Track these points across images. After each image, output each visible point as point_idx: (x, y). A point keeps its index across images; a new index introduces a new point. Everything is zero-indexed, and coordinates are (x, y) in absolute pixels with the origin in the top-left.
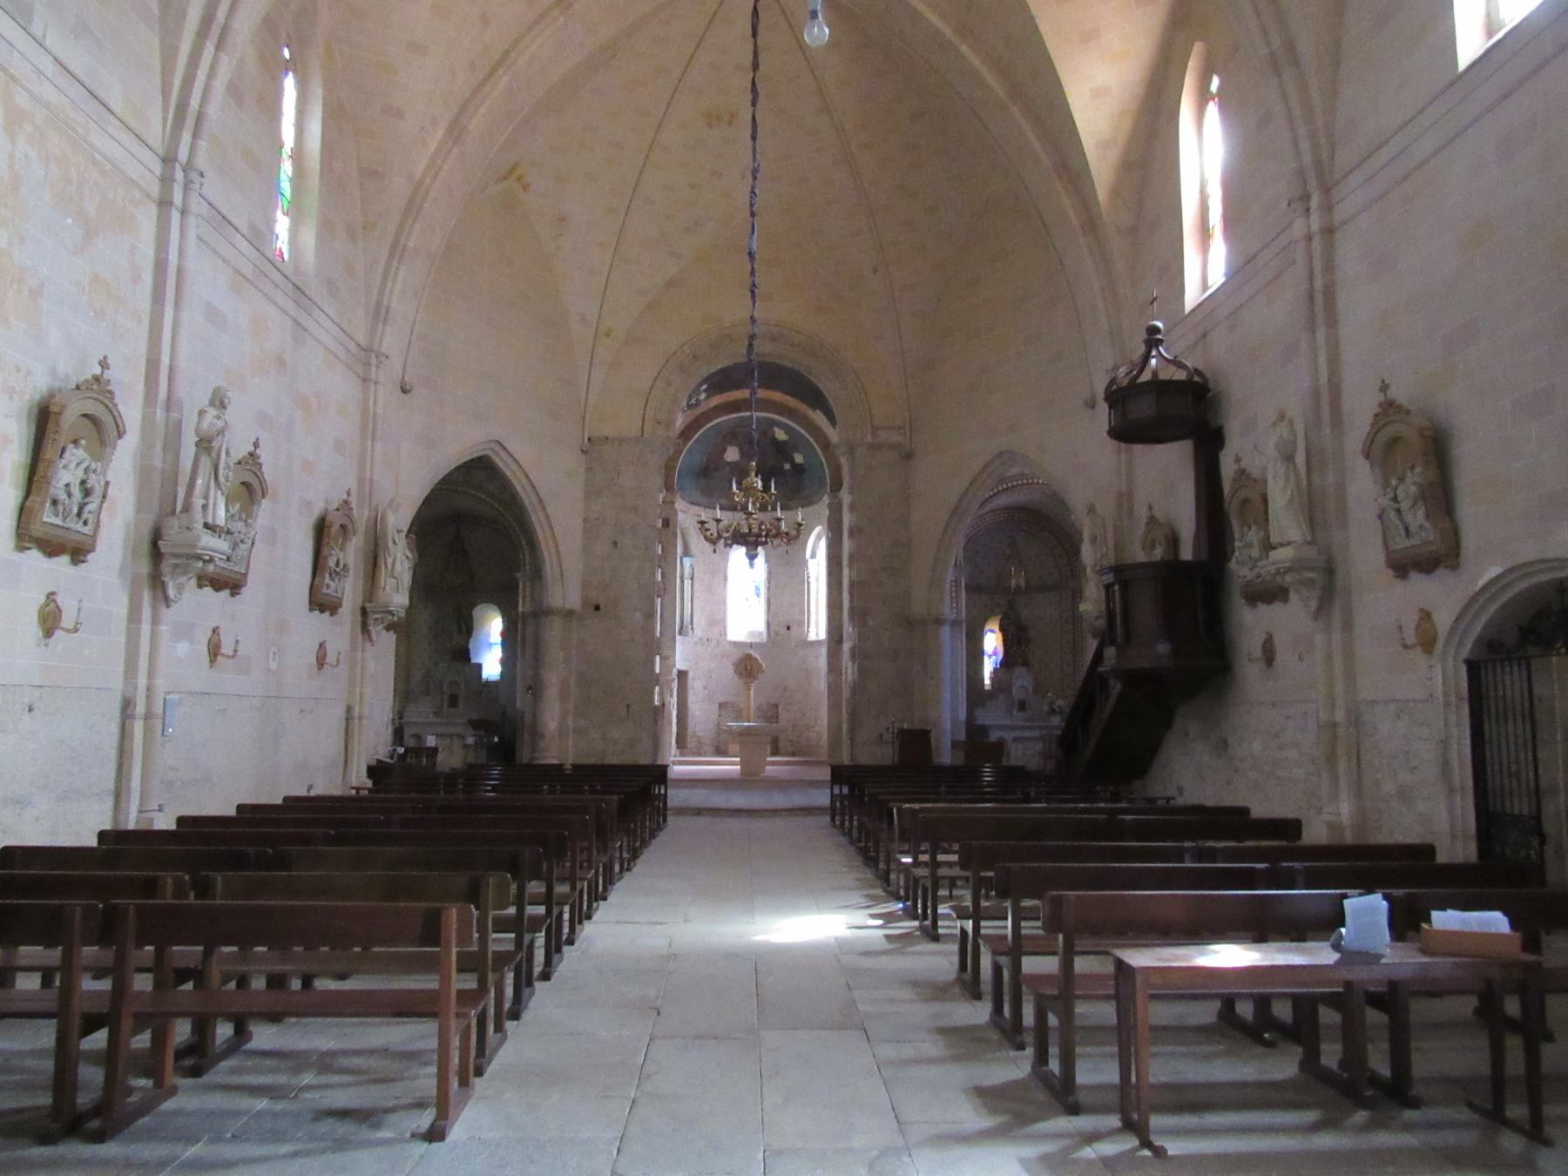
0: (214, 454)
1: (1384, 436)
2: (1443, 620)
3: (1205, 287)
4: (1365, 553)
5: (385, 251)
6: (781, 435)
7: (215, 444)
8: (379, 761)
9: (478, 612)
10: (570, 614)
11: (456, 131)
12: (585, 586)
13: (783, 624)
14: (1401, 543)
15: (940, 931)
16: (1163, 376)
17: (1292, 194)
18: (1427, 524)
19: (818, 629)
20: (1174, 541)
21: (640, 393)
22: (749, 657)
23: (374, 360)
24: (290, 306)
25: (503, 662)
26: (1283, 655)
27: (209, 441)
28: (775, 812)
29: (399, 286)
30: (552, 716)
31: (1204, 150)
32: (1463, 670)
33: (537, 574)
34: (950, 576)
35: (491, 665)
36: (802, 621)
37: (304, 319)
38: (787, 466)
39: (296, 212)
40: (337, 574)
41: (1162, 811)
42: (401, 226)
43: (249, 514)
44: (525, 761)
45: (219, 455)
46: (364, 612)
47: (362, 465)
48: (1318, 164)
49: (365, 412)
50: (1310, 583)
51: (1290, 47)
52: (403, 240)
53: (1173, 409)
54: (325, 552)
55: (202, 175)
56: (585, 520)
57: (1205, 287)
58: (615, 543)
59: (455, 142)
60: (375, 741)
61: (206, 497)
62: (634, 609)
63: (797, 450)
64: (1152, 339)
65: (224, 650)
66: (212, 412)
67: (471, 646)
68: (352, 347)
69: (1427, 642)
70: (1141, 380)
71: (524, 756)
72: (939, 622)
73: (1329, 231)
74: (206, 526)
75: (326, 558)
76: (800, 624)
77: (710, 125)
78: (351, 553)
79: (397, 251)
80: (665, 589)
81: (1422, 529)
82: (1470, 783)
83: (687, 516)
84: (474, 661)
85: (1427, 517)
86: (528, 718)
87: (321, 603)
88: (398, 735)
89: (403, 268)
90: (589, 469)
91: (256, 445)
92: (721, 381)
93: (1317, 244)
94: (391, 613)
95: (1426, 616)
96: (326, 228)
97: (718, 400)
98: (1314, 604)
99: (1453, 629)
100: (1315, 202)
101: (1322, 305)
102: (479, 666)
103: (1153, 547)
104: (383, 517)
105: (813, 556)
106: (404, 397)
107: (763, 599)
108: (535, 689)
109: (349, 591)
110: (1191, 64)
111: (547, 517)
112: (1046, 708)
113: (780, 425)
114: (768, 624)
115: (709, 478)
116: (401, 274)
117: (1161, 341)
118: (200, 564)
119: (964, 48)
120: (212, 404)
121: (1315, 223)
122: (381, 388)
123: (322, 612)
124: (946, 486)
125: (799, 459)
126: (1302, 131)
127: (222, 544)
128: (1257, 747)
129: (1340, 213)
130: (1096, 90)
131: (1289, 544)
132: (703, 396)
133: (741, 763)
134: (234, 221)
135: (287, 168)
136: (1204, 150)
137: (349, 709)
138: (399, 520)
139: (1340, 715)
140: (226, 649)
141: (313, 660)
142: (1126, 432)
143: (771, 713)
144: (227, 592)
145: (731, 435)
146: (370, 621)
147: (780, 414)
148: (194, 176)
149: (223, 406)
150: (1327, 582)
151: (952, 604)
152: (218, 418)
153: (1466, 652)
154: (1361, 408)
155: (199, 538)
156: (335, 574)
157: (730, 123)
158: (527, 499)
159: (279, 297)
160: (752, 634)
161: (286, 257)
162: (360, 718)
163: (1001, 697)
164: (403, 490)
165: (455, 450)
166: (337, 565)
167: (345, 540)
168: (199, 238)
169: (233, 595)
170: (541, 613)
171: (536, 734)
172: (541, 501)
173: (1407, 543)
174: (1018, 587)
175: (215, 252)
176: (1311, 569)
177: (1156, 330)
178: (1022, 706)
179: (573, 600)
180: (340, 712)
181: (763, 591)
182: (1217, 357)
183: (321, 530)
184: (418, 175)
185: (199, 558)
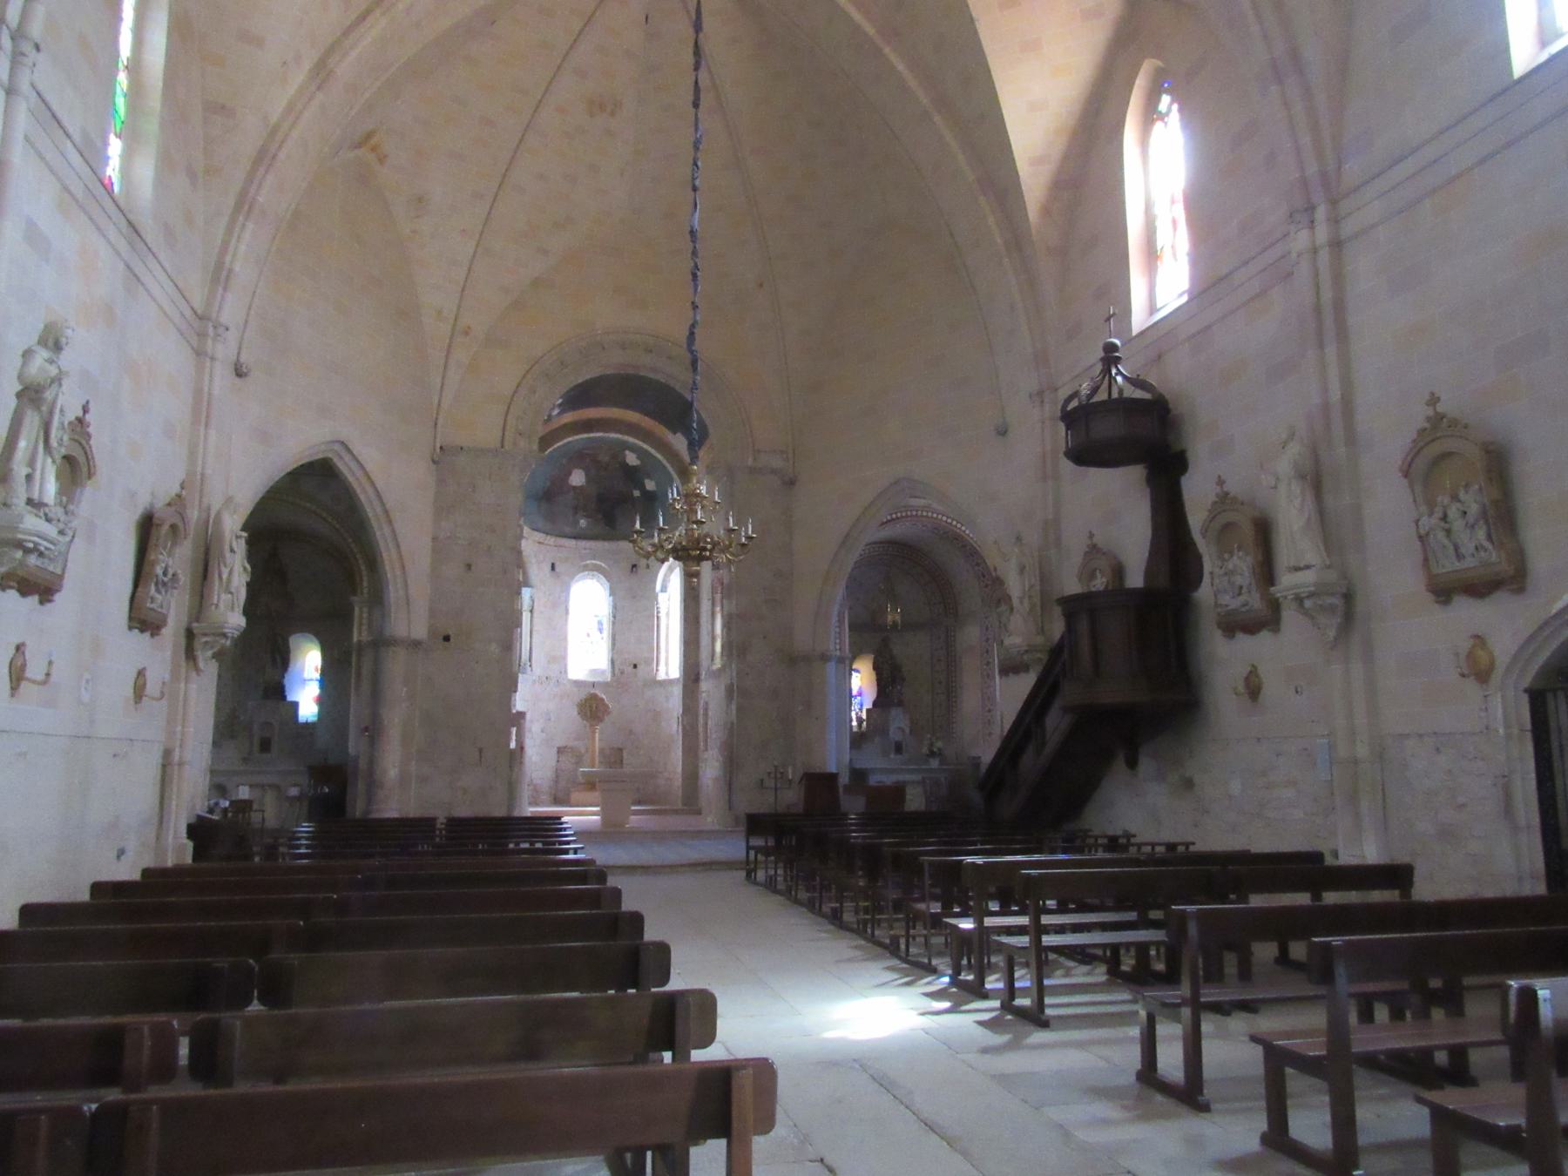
0: (44, 408)
1: (1436, 449)
2: (1503, 646)
3: (1152, 309)
4: (1392, 577)
5: (231, 201)
6: (632, 459)
7: (48, 395)
8: (199, 817)
9: (294, 640)
10: (416, 644)
11: (322, 72)
12: (433, 613)
13: (630, 664)
14: (1447, 565)
15: (1049, 1012)
16: (1126, 394)
17: (1271, 211)
18: (1487, 544)
19: (670, 665)
20: (1119, 572)
21: (498, 403)
22: (594, 697)
23: (211, 331)
24: (123, 246)
25: (320, 701)
26: (1273, 688)
27: (37, 392)
28: (673, 868)
29: (243, 248)
30: (391, 763)
31: (1159, 166)
32: (1525, 699)
33: (377, 599)
34: (836, 609)
35: (307, 700)
36: (652, 659)
37: (139, 269)
38: (637, 493)
39: (131, 137)
40: (164, 584)
41: (1162, 862)
42: (250, 179)
43: (71, 500)
44: (358, 814)
45: (51, 413)
46: (190, 635)
47: (192, 454)
48: (1324, 175)
49: (198, 393)
50: (1331, 609)
51: (1295, 55)
52: (252, 191)
53: (1135, 431)
54: (152, 556)
55: (38, 48)
56: (435, 539)
57: (1152, 309)
58: (469, 566)
59: (319, 88)
60: (192, 794)
61: (31, 463)
62: (485, 640)
63: (649, 477)
64: (1110, 357)
65: (29, 674)
66: (42, 354)
67: (286, 682)
68: (188, 313)
69: (1481, 674)
70: (1096, 399)
71: (357, 809)
72: (825, 658)
73: (1337, 245)
74: (30, 502)
75: (153, 564)
76: (649, 662)
77: (592, 115)
78: (176, 560)
79: (244, 204)
80: (511, 622)
81: (1475, 548)
82: (1536, 820)
83: (535, 547)
84: (290, 698)
85: (1489, 537)
86: (363, 764)
87: (143, 621)
88: (220, 789)
89: (250, 226)
90: (441, 482)
91: (85, 410)
92: (580, 396)
93: (1324, 256)
94: (225, 635)
95: (1479, 640)
96: (166, 162)
97: (569, 417)
98: (1332, 633)
99: (1515, 658)
100: (1321, 213)
101: (1330, 321)
102: (295, 705)
103: (1092, 576)
104: (219, 514)
105: (664, 589)
106: (237, 380)
107: (606, 633)
108: (373, 731)
109: (174, 607)
110: (1138, 82)
111: (393, 531)
112: (925, 750)
113: (634, 449)
114: (613, 662)
115: (550, 503)
116: (247, 235)
117: (1119, 358)
118: (19, 554)
119: (887, 50)
120: (43, 342)
121: (1322, 234)
122: (218, 365)
123: (142, 631)
124: (836, 519)
125: (650, 485)
126: (1306, 140)
127: (51, 530)
128: (1235, 787)
129: (1347, 229)
130: (1034, 101)
131: (1308, 567)
132: (556, 412)
133: (603, 813)
134: (65, 123)
135: (122, 79)
136: (1159, 166)
137: (167, 753)
138: (232, 525)
139: (1362, 751)
140: (35, 670)
141: (129, 691)
142: (1086, 454)
143: (615, 757)
144: (36, 598)
145: (579, 457)
146: (198, 644)
147: (636, 437)
148: (27, 48)
149: (58, 347)
150: (1345, 608)
151: (836, 637)
152: (51, 361)
153: (1527, 681)
154: (1388, 431)
155: (21, 517)
156: (162, 585)
157: (613, 114)
158: (371, 511)
159: (112, 234)
160: (594, 672)
161: (116, 188)
162: (181, 764)
163: (877, 740)
164: (237, 484)
165: (298, 443)
166: (165, 574)
167: (174, 544)
168: (27, 139)
169: (41, 602)
170: (381, 642)
171: (373, 784)
172: (386, 512)
173: (1458, 565)
174: (895, 624)
175: (42, 158)
176: (1333, 594)
177: (1114, 347)
178: (898, 748)
179: (420, 631)
180: (156, 758)
181: (606, 626)
182: (1177, 377)
183: (147, 527)
184: (274, 119)
185: (19, 545)
